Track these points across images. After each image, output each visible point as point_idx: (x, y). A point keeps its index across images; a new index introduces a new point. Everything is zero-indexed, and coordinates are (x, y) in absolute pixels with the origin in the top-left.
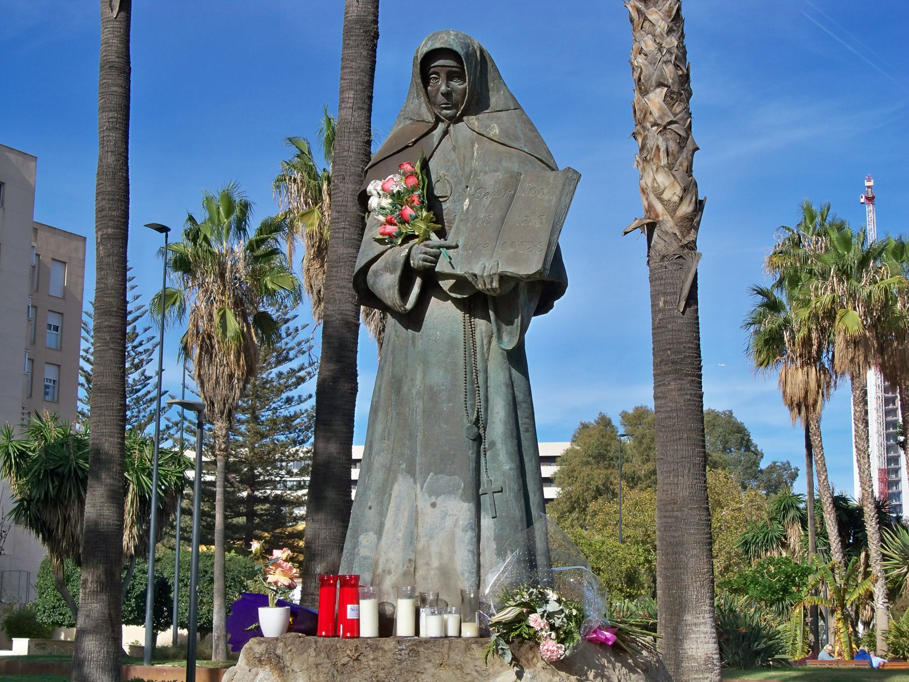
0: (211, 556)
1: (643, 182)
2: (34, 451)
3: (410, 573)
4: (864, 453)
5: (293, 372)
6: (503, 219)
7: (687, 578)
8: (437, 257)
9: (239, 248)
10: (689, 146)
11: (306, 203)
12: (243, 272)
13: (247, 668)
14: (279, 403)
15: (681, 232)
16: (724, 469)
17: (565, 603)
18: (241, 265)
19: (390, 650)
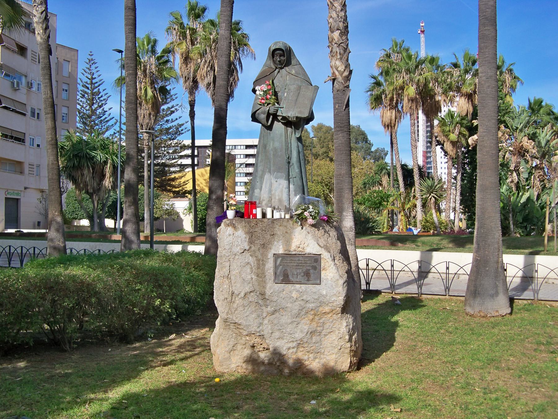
2: (67, 146)
3: (270, 200)
4: (415, 147)
5: (169, 108)
6: (297, 100)
7: (345, 200)
8: (277, 110)
10: (348, 51)
11: (179, 39)
12: (154, 70)
16: (356, 151)
18: (153, 67)
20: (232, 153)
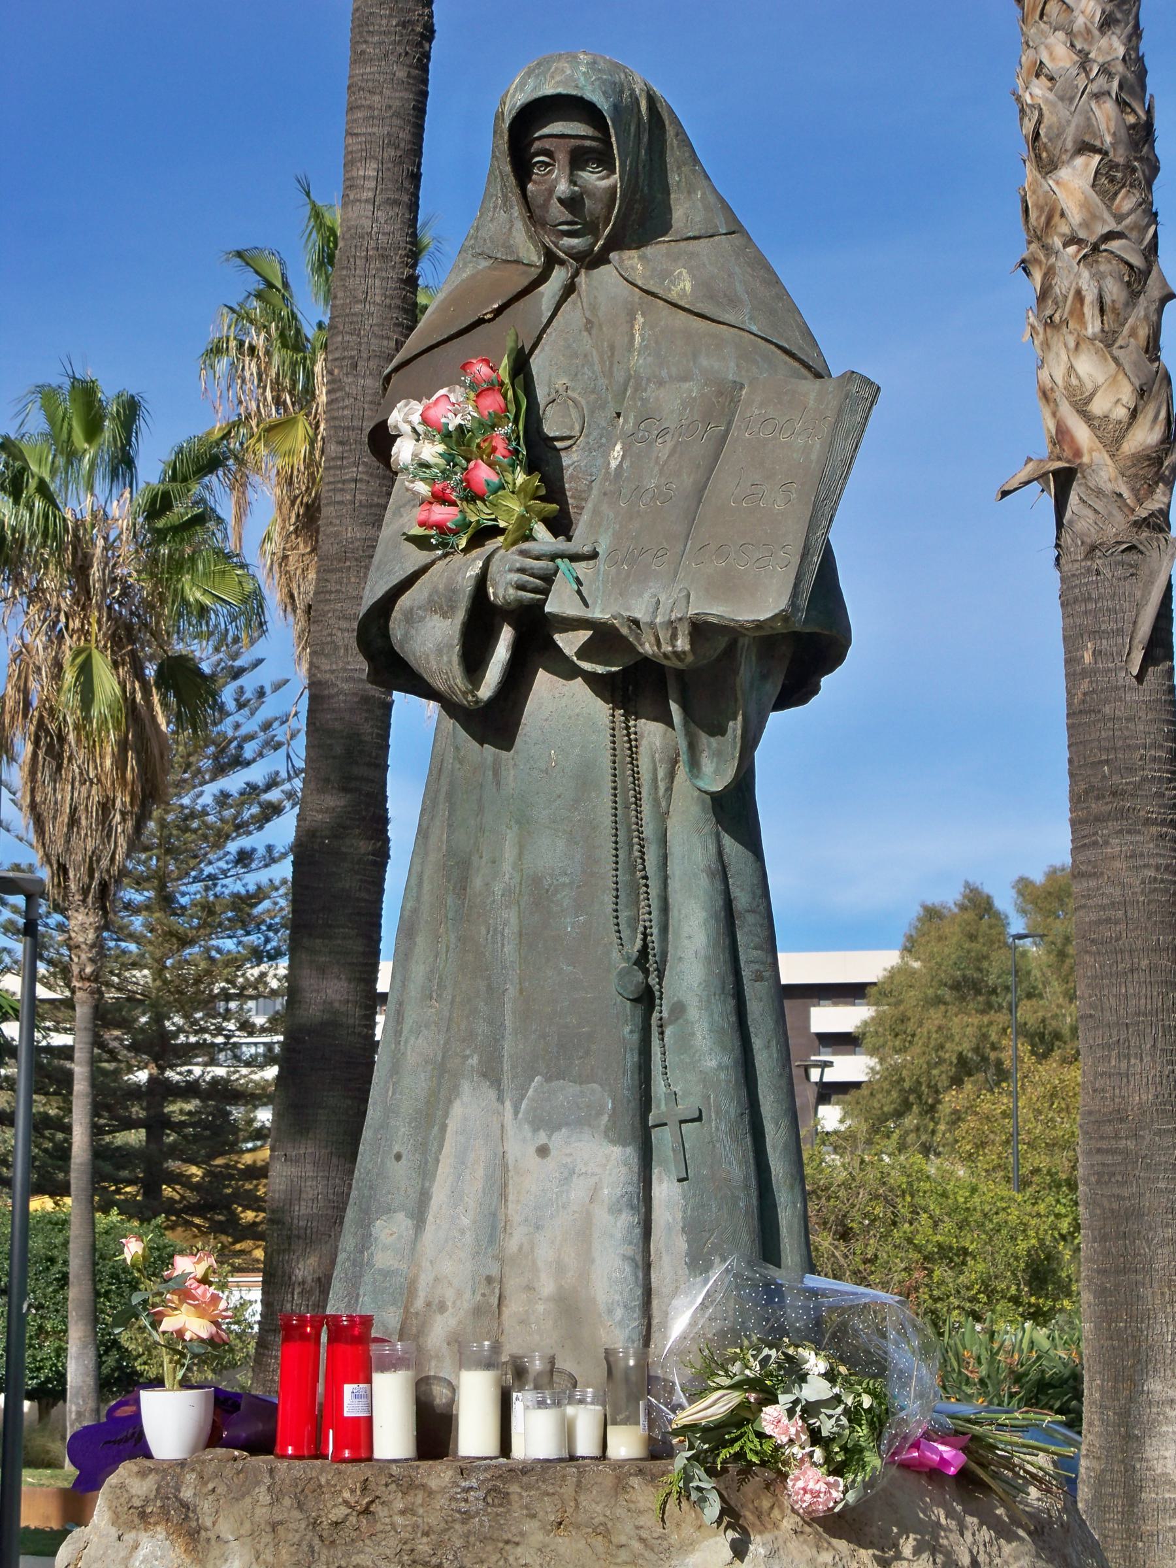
0: (63, 1224)
1: (1044, 375)
3: (491, 1306)
5: (252, 791)
6: (700, 490)
8: (548, 579)
9: (123, 510)
10: (1153, 290)
11: (278, 402)
13: (114, 1532)
14: (222, 864)
15: (1135, 491)
17: (846, 1380)
18: (126, 549)
19: (443, 1490)
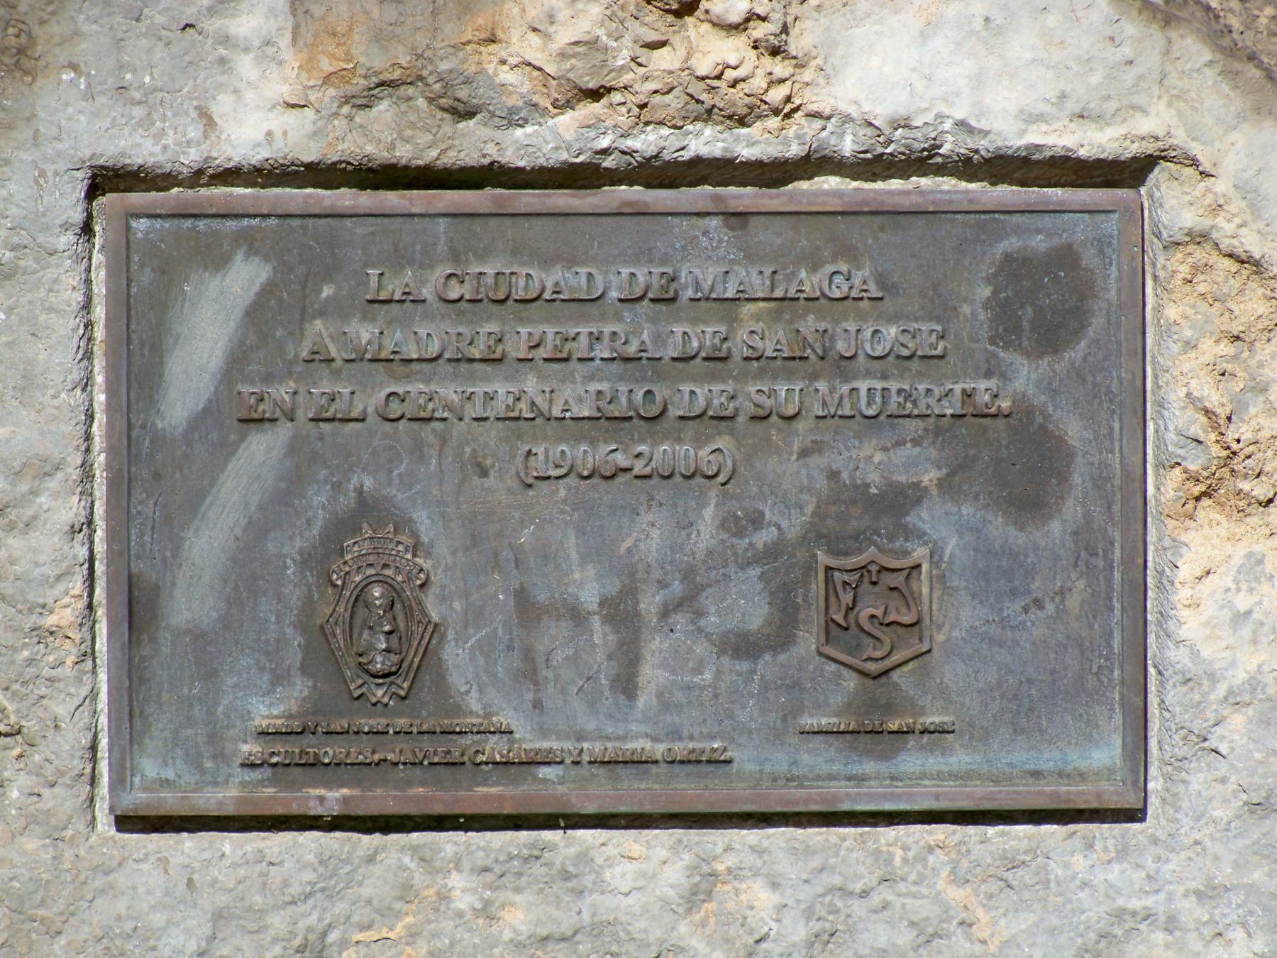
20: (1047, 359)
